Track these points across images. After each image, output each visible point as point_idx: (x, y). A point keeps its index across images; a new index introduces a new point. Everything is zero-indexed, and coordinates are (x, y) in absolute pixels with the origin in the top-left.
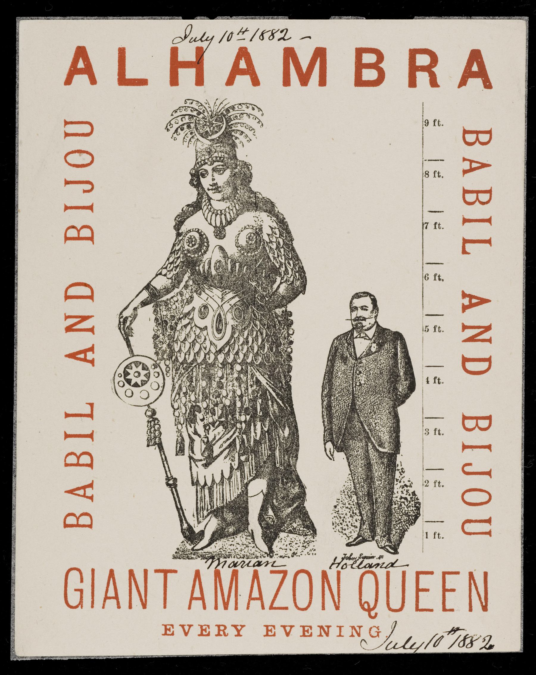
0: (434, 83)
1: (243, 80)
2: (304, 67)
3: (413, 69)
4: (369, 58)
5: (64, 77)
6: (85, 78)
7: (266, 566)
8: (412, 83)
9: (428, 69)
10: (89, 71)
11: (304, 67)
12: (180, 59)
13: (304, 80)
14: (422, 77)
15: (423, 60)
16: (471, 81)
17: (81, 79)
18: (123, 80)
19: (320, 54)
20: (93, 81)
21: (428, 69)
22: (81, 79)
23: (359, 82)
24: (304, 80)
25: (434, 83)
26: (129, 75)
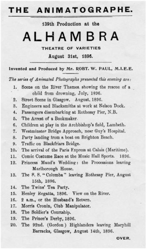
0: (105, 39)
1: (62, 40)
2: (76, 37)
3: (100, 36)
4: (90, 34)
5: (111, 39)
6: (116, 39)
7: (73, 219)
8: (100, 40)
9: (99, 10)
10: (29, 38)
11: (76, 37)
12: (48, 35)
13: (76, 40)
14: (103, 38)
15: (103, 34)
16: (26, 39)
17: (114, 39)
18: (35, 40)
19: (79, 33)
20: (65, 40)
21: (99, 10)
22: (27, 40)
23: (88, 40)
24: (76, 40)
25: (105, 39)
26: (37, 39)
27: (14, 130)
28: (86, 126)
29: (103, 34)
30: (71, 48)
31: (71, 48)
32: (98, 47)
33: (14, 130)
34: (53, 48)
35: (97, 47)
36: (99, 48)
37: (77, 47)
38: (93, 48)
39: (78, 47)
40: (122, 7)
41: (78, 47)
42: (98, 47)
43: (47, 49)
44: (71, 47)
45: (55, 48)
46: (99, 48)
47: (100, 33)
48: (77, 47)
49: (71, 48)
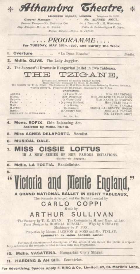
3: (54, 204)
14: (37, 216)
17: (32, 216)
27: (24, 225)
28: (110, 156)
29: (55, 203)
30: (28, 46)
31: (28, 46)
32: (39, 133)
33: (24, 225)
34: (48, 88)
35: (37, 133)
36: (45, 113)
37: (32, 252)
38: (46, 194)
39: (33, 252)
40: (36, 216)
41: (33, 252)
42: (39, 133)
43: (50, 216)
44: (36, 122)
45: (43, 194)
46: (45, 113)
47: (54, 202)
48: (32, 252)
49: (64, 155)
